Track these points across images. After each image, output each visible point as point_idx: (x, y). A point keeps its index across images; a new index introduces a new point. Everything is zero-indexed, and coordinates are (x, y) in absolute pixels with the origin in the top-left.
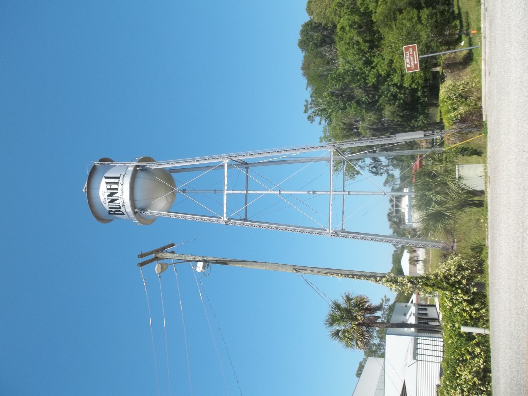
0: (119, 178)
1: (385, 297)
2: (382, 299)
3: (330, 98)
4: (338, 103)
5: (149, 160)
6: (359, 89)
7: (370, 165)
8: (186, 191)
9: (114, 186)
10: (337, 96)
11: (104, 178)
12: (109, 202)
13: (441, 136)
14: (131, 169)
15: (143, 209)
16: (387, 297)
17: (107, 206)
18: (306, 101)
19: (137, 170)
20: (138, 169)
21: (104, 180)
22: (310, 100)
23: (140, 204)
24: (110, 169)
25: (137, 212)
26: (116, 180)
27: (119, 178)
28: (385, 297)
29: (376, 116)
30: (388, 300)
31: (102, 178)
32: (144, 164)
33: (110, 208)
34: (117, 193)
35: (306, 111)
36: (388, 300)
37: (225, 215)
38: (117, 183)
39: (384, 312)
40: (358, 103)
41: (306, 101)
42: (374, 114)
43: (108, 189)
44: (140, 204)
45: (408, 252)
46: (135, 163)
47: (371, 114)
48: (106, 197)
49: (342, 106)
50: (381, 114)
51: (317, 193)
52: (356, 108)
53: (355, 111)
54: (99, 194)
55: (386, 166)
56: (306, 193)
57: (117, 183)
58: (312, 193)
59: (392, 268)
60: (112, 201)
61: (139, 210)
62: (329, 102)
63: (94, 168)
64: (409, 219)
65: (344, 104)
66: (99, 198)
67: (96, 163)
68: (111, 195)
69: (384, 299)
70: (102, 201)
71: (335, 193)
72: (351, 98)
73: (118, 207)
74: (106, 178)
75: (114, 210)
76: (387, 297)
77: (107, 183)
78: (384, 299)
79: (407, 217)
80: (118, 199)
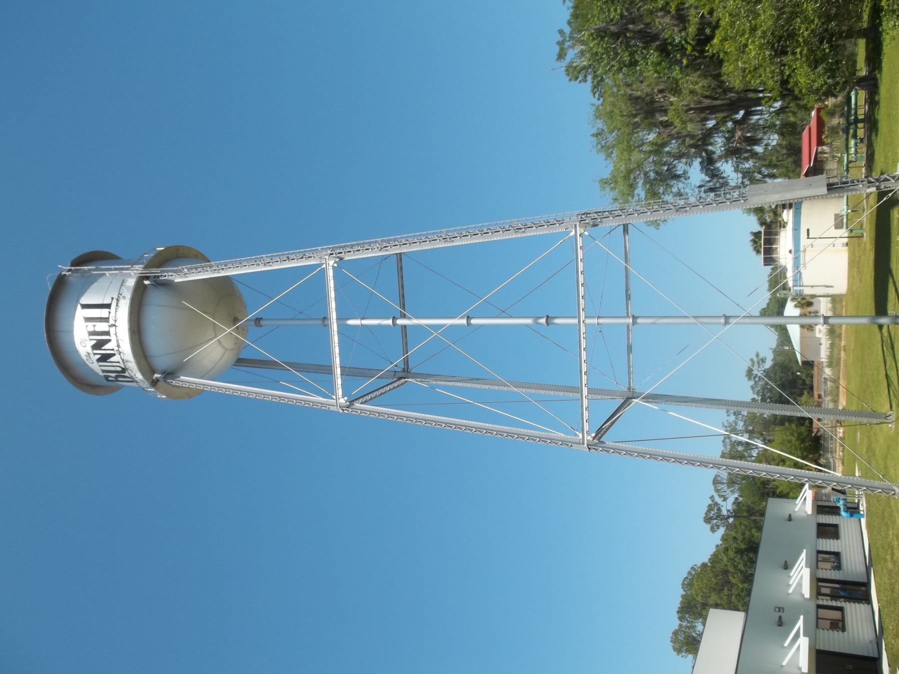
0: (108, 306)
1: (757, 355)
2: (752, 360)
3: (598, 44)
4: (617, 54)
5: (174, 256)
6: (663, 17)
7: (700, 187)
8: (262, 323)
9: (102, 327)
10: (616, 36)
11: (79, 307)
12: (99, 360)
13: (878, 188)
14: (131, 282)
15: (170, 374)
16: (761, 356)
17: (96, 367)
18: (561, 32)
19: (146, 286)
20: (146, 282)
21: (81, 314)
22: (567, 30)
23: (162, 361)
24: (92, 283)
25: (157, 380)
26: (104, 313)
27: (108, 306)
28: (757, 355)
29: (704, 82)
30: (763, 360)
31: (76, 307)
32: (156, 271)
33: (104, 371)
34: (109, 341)
35: (561, 56)
36: (763, 360)
37: (340, 392)
38: (106, 320)
39: (756, 382)
40: (664, 50)
41: (561, 32)
42: (704, 76)
43: (92, 333)
44: (162, 361)
45: (796, 306)
46: (138, 269)
47: (694, 76)
48: (90, 350)
49: (627, 59)
50: (719, 75)
51: (557, 321)
52: (659, 64)
53: (656, 72)
54: (74, 343)
55: (737, 187)
56: (529, 321)
57: (106, 320)
58: (543, 321)
59: (767, 301)
60: (104, 358)
61: (161, 375)
62: (596, 53)
63: (61, 283)
64: (795, 280)
65: (632, 54)
66: (77, 352)
67: (65, 269)
68: (99, 345)
69: (755, 359)
70: (85, 358)
71: (601, 321)
72: (648, 37)
73: (119, 369)
74: (85, 306)
75: (113, 375)
76: (761, 356)
77: (88, 320)
78: (755, 359)
79: (790, 274)
80: (114, 355)
